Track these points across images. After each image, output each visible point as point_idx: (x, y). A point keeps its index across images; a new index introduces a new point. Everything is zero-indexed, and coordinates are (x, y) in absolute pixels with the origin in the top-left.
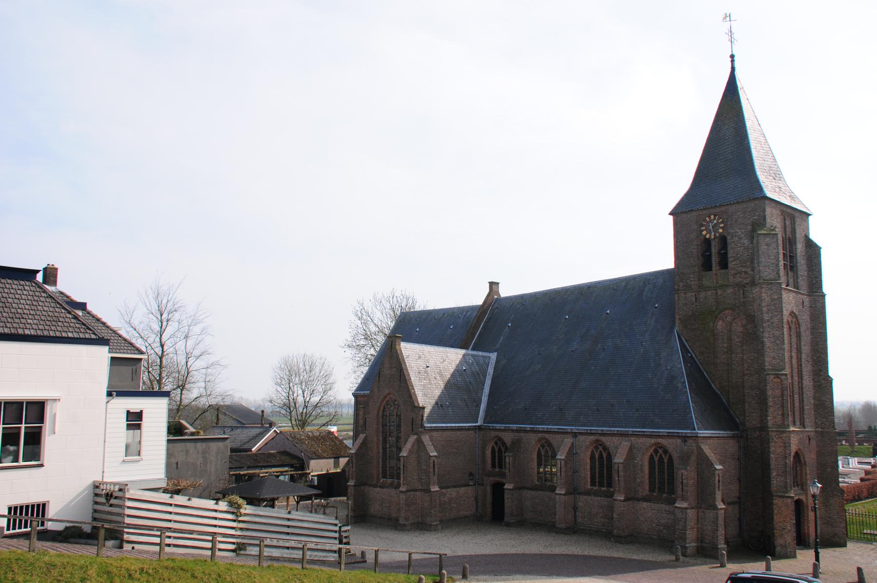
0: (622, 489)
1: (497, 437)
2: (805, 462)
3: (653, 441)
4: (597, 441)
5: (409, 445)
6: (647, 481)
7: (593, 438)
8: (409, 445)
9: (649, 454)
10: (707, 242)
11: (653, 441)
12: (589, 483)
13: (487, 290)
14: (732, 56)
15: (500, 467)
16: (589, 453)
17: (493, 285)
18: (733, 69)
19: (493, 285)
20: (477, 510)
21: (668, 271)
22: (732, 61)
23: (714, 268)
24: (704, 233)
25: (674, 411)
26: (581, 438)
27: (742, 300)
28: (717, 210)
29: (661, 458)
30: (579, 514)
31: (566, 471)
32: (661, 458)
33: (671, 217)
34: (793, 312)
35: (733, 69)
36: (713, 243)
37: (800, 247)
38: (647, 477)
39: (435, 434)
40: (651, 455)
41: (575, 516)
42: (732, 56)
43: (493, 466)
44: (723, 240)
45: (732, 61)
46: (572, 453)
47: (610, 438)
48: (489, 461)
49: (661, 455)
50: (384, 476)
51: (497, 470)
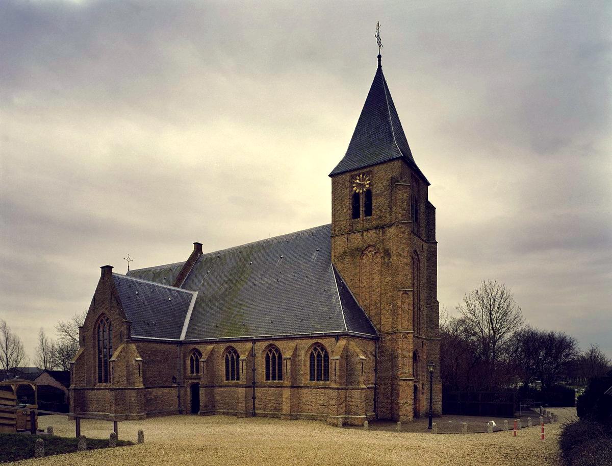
0: (289, 379)
1: (195, 349)
2: (419, 360)
3: (314, 341)
4: (271, 345)
5: (117, 353)
6: (309, 373)
7: (267, 343)
8: (117, 353)
9: (310, 352)
10: (356, 197)
11: (314, 341)
12: (265, 378)
13: (191, 249)
14: (379, 57)
15: (198, 372)
16: (265, 355)
17: (198, 247)
18: (380, 66)
19: (198, 247)
20: (179, 406)
21: (327, 226)
22: (379, 61)
23: (361, 216)
24: (355, 189)
25: (330, 318)
26: (259, 344)
27: (382, 238)
28: (365, 170)
29: (319, 354)
30: (256, 402)
31: (246, 369)
32: (319, 354)
33: (330, 179)
34: (416, 251)
35: (380, 66)
36: (361, 196)
37: (422, 207)
38: (308, 370)
39: (141, 344)
40: (312, 352)
41: (254, 404)
42: (379, 57)
43: (192, 372)
44: (368, 194)
45: (379, 61)
46: (252, 355)
47: (281, 342)
48: (189, 368)
49: (319, 352)
50: (100, 381)
51: (195, 374)
